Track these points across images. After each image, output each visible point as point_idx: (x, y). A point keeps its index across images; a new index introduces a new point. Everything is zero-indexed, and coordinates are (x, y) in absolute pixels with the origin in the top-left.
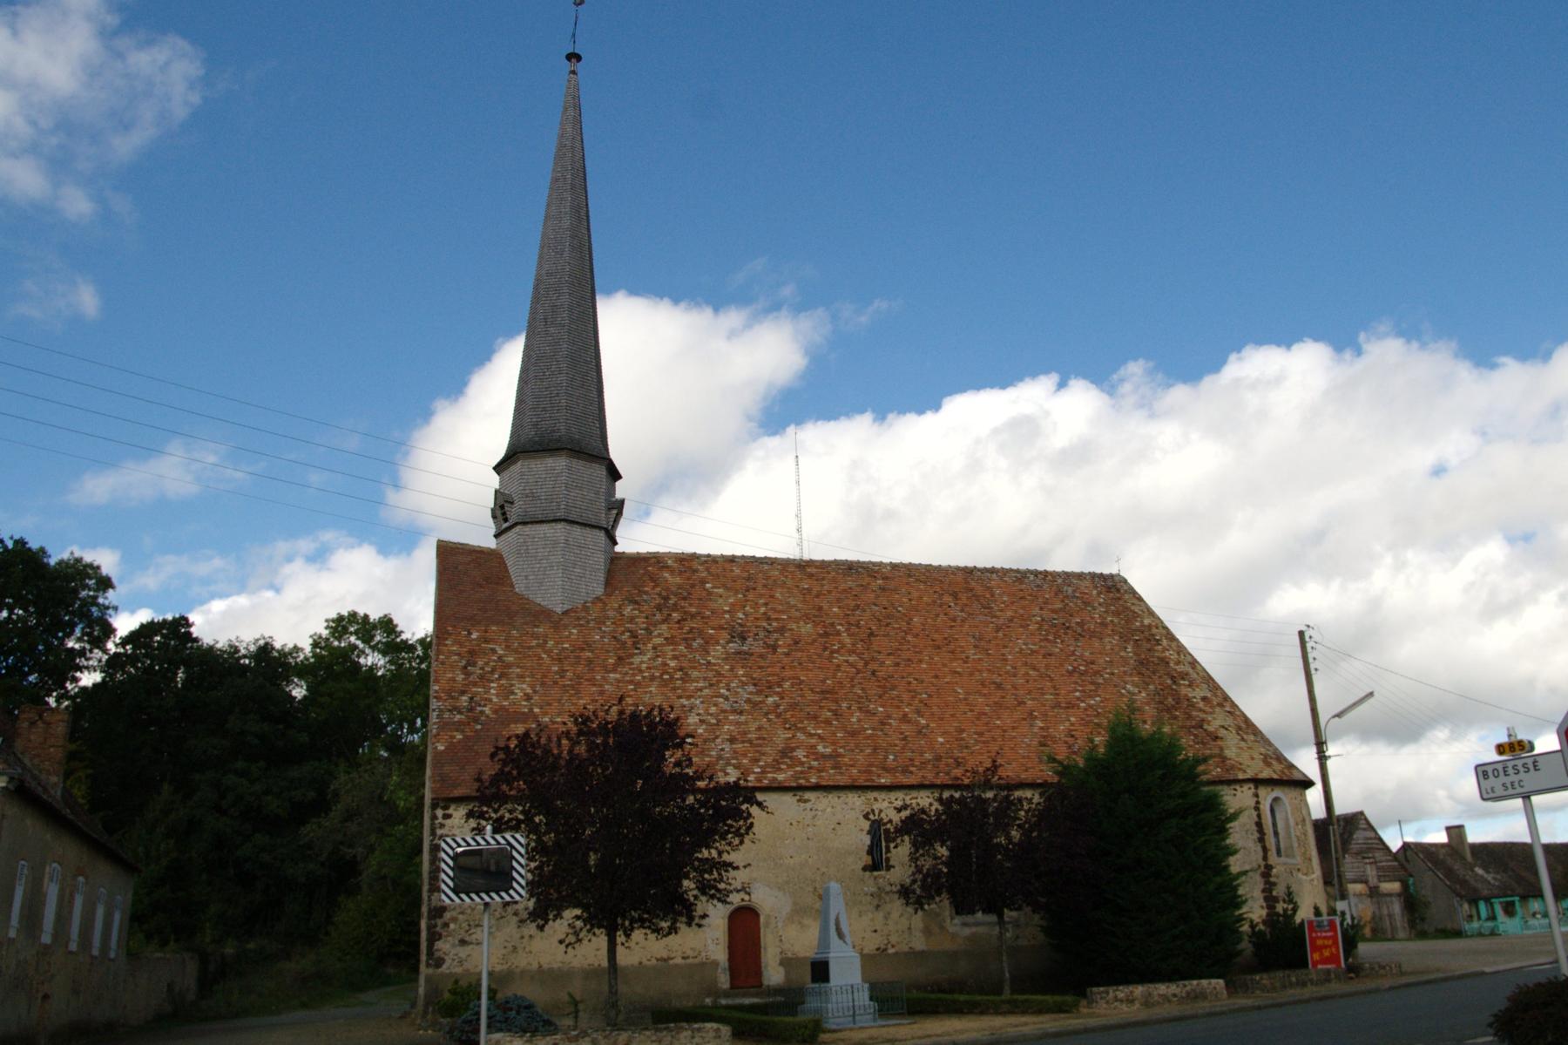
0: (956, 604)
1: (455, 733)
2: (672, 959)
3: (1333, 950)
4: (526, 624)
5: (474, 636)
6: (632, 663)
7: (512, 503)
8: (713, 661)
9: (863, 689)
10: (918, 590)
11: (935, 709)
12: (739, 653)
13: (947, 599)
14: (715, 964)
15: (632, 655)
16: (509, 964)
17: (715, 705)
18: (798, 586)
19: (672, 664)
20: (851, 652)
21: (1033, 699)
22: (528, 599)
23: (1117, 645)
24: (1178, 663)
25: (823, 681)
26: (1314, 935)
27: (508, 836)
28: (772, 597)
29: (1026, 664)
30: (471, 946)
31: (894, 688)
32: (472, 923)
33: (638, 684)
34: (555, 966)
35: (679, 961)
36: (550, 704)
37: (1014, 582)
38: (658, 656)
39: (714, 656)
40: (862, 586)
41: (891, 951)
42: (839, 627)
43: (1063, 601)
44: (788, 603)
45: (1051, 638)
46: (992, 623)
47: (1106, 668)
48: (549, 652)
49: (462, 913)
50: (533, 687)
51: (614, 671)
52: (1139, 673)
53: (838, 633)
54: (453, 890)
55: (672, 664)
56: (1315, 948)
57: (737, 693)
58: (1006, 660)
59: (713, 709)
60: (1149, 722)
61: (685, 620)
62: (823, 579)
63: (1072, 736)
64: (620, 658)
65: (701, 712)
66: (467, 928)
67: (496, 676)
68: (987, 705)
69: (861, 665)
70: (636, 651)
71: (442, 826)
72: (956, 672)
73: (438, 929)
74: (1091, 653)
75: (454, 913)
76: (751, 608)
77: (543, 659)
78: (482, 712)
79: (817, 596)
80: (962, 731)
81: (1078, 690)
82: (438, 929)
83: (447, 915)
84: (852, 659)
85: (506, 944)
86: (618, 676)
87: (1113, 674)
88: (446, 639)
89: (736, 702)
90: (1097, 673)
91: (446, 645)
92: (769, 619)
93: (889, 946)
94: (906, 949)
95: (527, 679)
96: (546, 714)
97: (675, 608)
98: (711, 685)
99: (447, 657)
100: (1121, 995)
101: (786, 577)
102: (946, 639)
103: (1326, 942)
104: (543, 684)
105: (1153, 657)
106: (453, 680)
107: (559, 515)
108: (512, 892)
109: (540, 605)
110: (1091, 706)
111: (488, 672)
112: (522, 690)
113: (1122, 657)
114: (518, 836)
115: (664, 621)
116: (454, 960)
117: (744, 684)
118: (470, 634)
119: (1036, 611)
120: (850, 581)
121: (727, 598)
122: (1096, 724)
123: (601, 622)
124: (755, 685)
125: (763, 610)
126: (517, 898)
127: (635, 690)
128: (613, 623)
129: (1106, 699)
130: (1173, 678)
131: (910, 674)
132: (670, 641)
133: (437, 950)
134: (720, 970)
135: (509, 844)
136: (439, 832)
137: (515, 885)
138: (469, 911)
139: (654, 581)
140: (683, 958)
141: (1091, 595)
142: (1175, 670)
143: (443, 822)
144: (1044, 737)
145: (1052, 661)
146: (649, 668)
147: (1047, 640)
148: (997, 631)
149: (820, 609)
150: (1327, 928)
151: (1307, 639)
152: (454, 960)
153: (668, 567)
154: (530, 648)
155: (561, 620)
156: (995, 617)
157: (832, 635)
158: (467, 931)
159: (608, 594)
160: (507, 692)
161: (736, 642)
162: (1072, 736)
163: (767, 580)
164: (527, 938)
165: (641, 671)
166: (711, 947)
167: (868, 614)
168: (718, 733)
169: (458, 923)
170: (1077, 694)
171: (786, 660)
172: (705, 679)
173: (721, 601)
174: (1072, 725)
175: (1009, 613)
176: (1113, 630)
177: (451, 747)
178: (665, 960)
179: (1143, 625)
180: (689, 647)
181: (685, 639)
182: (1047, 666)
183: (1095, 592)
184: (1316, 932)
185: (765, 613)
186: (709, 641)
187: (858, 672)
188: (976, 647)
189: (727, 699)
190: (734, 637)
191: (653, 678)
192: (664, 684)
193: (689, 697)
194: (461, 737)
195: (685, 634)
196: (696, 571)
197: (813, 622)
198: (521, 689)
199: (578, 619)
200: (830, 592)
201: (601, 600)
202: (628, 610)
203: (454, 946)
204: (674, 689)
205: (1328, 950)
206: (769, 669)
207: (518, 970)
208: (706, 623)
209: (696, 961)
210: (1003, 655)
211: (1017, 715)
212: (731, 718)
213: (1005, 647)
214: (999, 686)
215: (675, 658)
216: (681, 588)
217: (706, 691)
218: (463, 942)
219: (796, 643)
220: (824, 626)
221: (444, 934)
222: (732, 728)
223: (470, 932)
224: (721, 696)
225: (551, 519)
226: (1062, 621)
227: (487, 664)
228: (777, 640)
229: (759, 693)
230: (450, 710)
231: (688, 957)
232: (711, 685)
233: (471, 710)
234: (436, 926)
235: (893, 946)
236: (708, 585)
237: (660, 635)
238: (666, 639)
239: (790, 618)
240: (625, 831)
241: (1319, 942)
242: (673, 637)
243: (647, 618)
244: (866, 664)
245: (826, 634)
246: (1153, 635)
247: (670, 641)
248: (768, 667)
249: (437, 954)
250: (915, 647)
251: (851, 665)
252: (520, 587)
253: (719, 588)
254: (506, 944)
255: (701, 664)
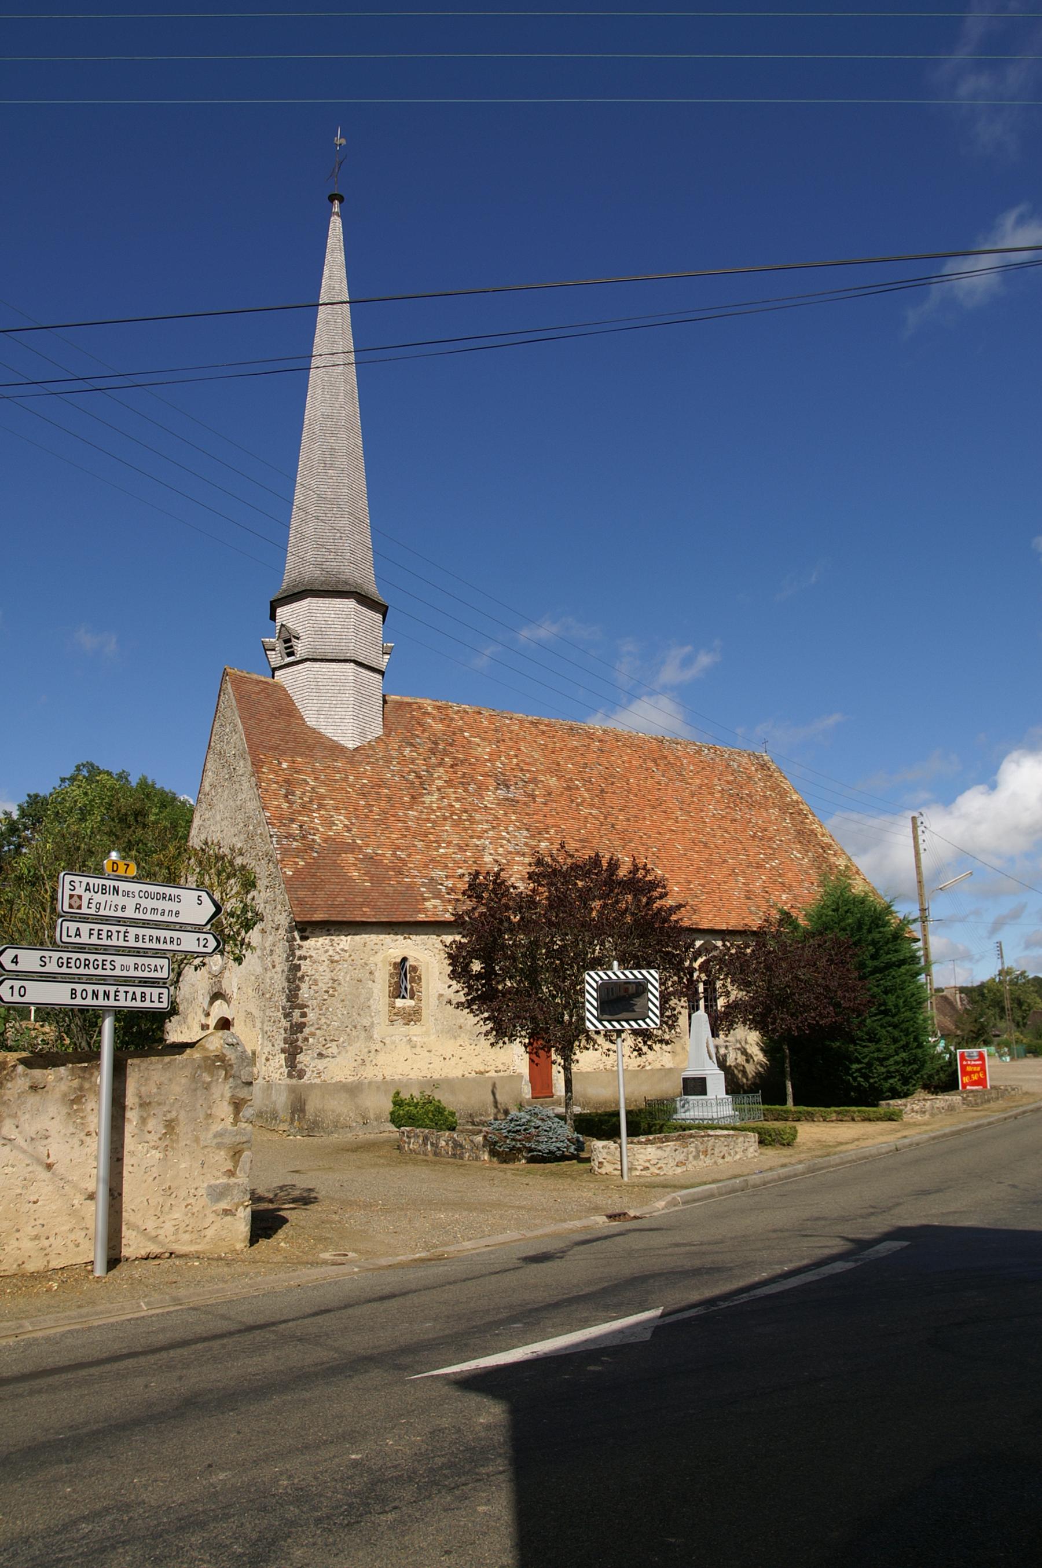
0: (658, 769)
1: (297, 860)
2: (487, 1072)
3: (981, 1075)
4: (326, 757)
5: (285, 765)
6: (424, 803)
7: (298, 638)
8: (489, 805)
9: (609, 840)
10: (627, 754)
11: (665, 862)
12: (507, 800)
13: (650, 764)
14: (520, 1076)
15: (422, 795)
16: (359, 1076)
17: (502, 846)
18: (535, 741)
19: (457, 805)
20: (592, 806)
21: (732, 858)
22: (319, 733)
23: (779, 816)
24: (823, 835)
25: (579, 830)
26: (965, 1063)
27: (644, 972)
28: (519, 749)
29: (720, 827)
30: (328, 1059)
31: (631, 840)
32: (328, 1038)
33: (434, 822)
34: (396, 1077)
35: (492, 1074)
36: (368, 837)
37: (695, 753)
38: (443, 797)
39: (488, 801)
40: (585, 746)
41: (648, 1068)
42: (577, 782)
43: (733, 774)
44: (532, 756)
45: (732, 806)
46: (687, 788)
47: (775, 836)
48: (351, 786)
49: (319, 1029)
50: (349, 818)
51: (411, 808)
52: (800, 842)
53: (578, 788)
54: (597, 1018)
55: (457, 805)
56: (965, 1073)
57: (516, 837)
58: (704, 822)
59: (501, 850)
60: (815, 884)
61: (457, 765)
62: (554, 737)
63: (767, 892)
64: (413, 797)
65: (492, 852)
66: (324, 1042)
67: (315, 806)
68: (701, 861)
69: (602, 818)
70: (424, 791)
71: (300, 947)
72: (673, 831)
73: (299, 1043)
74: (763, 822)
75: (312, 1029)
76: (506, 759)
77: (349, 793)
78: (313, 840)
79: (553, 753)
80: (690, 882)
81: (761, 853)
82: (299, 1043)
83: (307, 1030)
84: (594, 812)
85: (357, 1058)
86: (415, 813)
87: (781, 841)
88: (262, 767)
89: (517, 845)
90: (771, 839)
91: (264, 773)
92: (522, 770)
93: (647, 1064)
94: (659, 1066)
95: (342, 811)
96: (367, 845)
97: (445, 752)
98: (494, 827)
99: (269, 785)
100: (916, 1107)
101: (525, 732)
102: (657, 800)
103: (975, 1069)
104: (357, 817)
105: (805, 828)
106: (279, 807)
107: (348, 656)
108: (648, 1020)
109: (331, 740)
110: (774, 868)
111: (307, 802)
112: (341, 821)
113: (784, 827)
114: (652, 971)
115: (440, 765)
116: (313, 1071)
117: (519, 829)
118: (280, 763)
119: (716, 781)
120: (575, 740)
121: (484, 747)
122: (780, 883)
123: (388, 760)
124: (527, 830)
125: (515, 761)
126: (653, 1025)
127: (433, 828)
128: (398, 763)
129: (783, 863)
130: (822, 848)
131: (640, 829)
132: (449, 783)
133: (299, 1063)
134: (523, 1083)
135: (645, 978)
136: (298, 953)
137: (650, 1014)
138: (325, 1027)
139: (421, 726)
140: (496, 1071)
141: (751, 770)
142: (822, 841)
143: (301, 943)
144: (748, 891)
145: (738, 826)
146: (439, 808)
147: (729, 807)
148: (693, 797)
149: (558, 764)
150: (977, 1058)
151: (919, 824)
152: (313, 1071)
153: (429, 714)
154: (336, 781)
155: (354, 756)
156: (688, 784)
157: (573, 788)
158: (324, 1046)
159: (387, 735)
160: (330, 824)
161: (501, 789)
162: (767, 892)
163: (510, 733)
164: (373, 1051)
165: (434, 811)
166: (517, 1062)
167: (595, 772)
168: (510, 873)
169: (316, 1037)
170: (762, 856)
171: (546, 809)
172: (487, 821)
173: (480, 749)
174: (764, 882)
175: (698, 781)
176: (773, 803)
177: (297, 872)
178: (481, 1073)
179: (792, 801)
180: (466, 790)
181: (462, 783)
182: (735, 830)
183: (753, 768)
184: (967, 1060)
185: (517, 765)
186: (481, 787)
187: (602, 824)
188: (681, 809)
189: (509, 841)
190: (499, 784)
191: (445, 819)
192: (457, 824)
193: (479, 838)
194: (303, 863)
195: (460, 778)
196: (452, 719)
197: (557, 775)
198: (340, 820)
199: (368, 757)
200: (562, 749)
201: (382, 739)
202: (407, 751)
203: (313, 1058)
204: (465, 829)
205: (976, 1075)
206: (535, 816)
207: (366, 1081)
208: (474, 770)
209: (506, 1074)
210: (702, 818)
211: (725, 872)
212: (517, 859)
213: (702, 811)
214: (706, 845)
215: (457, 800)
216: (446, 735)
217: (491, 833)
218: (321, 1055)
219: (550, 794)
220: (566, 781)
221: (304, 1048)
222: (520, 868)
223: (326, 1046)
224: (504, 838)
225: (342, 658)
226: (736, 791)
227: (304, 793)
228: (534, 790)
229: (532, 837)
230: (286, 837)
231: (500, 1071)
232: (494, 827)
233: (304, 837)
234: (297, 1040)
235: (650, 1064)
236: (466, 734)
237: (440, 778)
238: (446, 781)
239: (538, 770)
240: (558, 962)
241: (969, 1069)
242: (451, 780)
243: (425, 760)
244: (606, 818)
245: (569, 788)
246: (801, 810)
247: (449, 783)
248: (534, 814)
249: (299, 1066)
250: (637, 805)
251: (595, 818)
252: (311, 721)
253: (475, 737)
254: (357, 1058)
255: (481, 808)
